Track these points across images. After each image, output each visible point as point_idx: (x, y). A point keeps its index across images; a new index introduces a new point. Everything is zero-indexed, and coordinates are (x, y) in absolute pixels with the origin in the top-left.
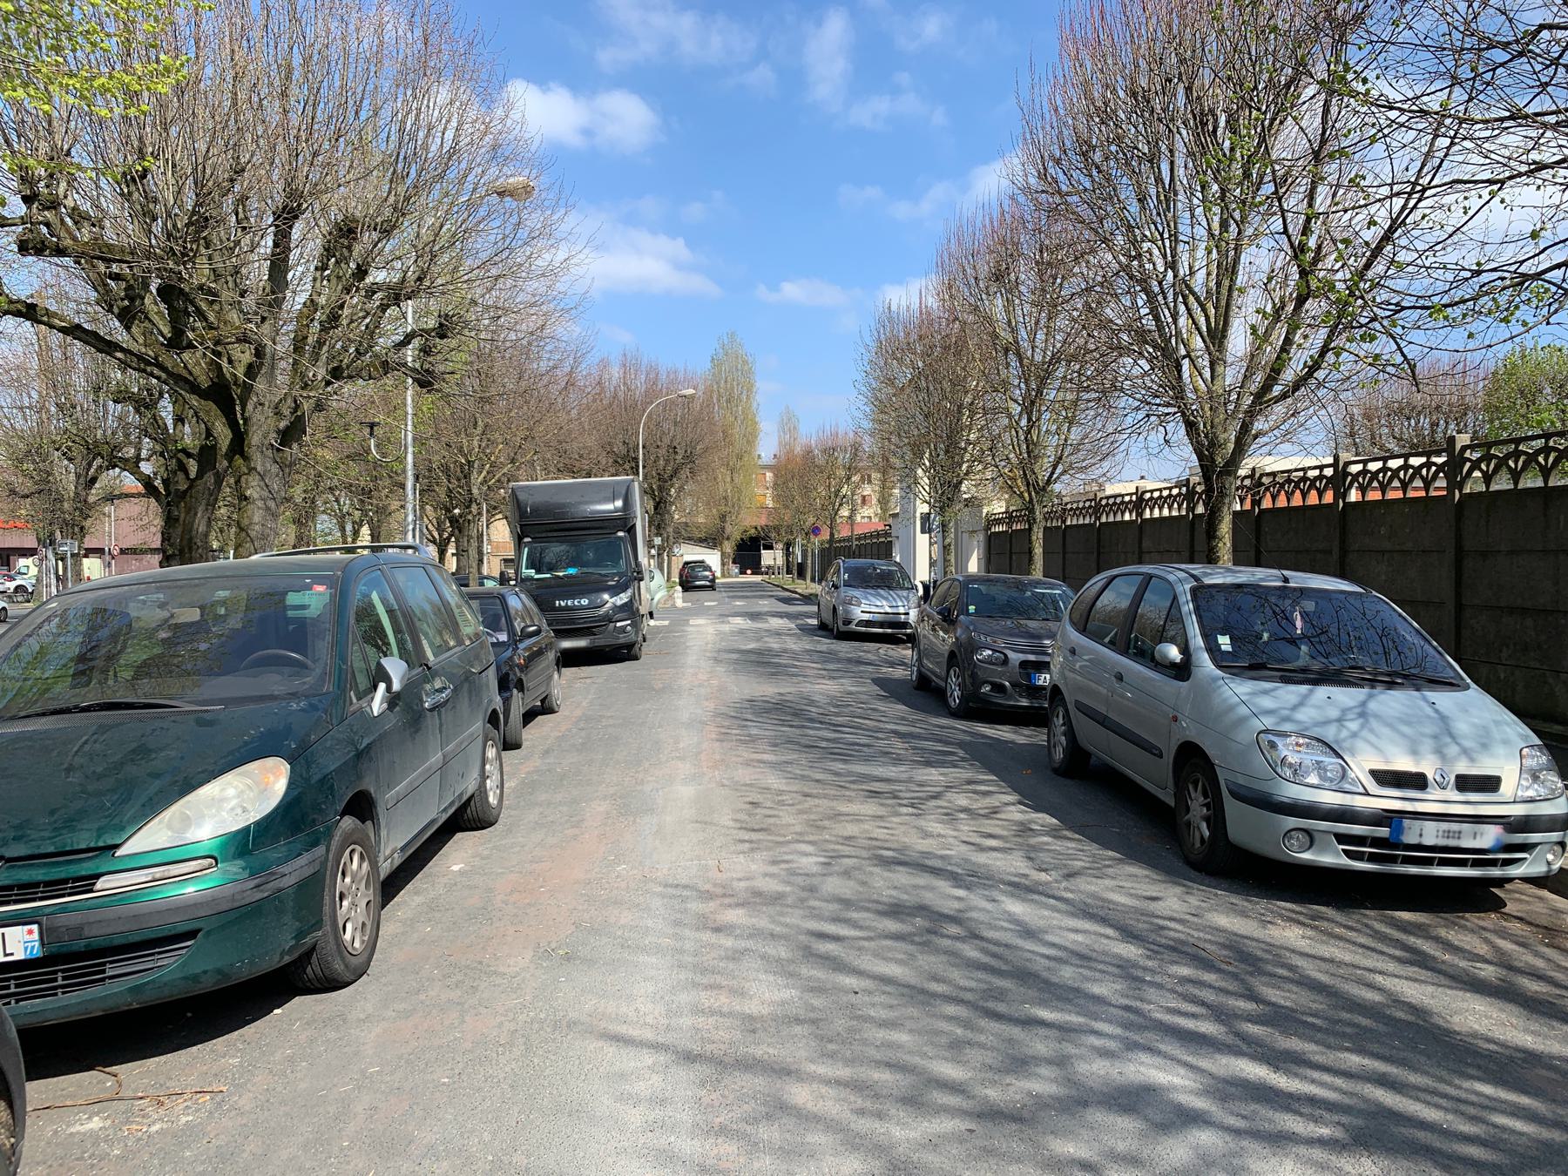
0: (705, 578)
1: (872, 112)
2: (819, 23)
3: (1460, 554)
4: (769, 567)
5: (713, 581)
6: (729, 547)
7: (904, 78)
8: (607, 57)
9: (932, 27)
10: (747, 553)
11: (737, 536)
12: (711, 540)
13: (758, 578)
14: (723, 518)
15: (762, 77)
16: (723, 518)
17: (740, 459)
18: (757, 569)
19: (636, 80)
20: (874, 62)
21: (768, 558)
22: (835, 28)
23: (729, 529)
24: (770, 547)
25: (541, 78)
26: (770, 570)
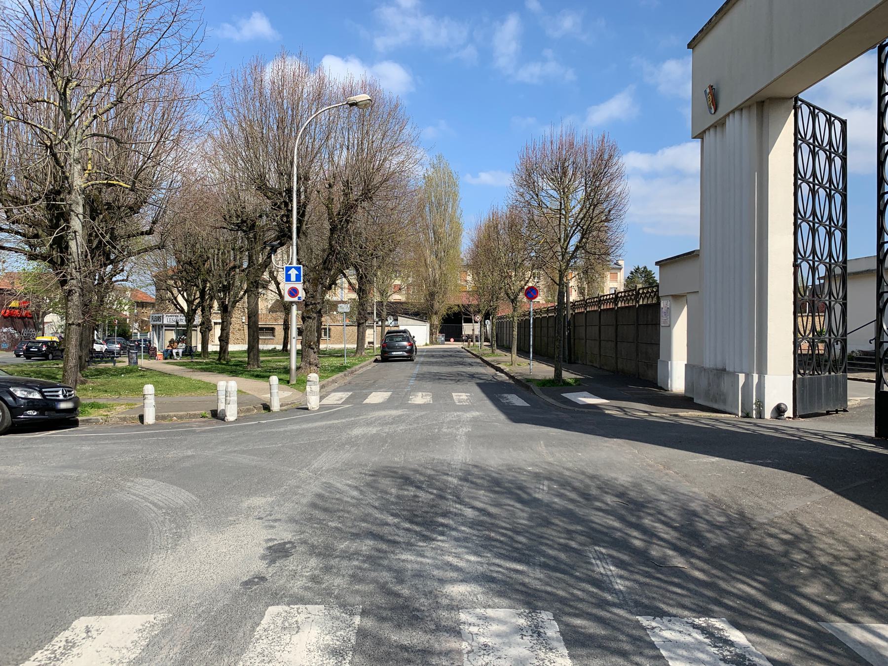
0: (402, 348)
1: (531, 73)
2: (503, 21)
3: (617, 326)
4: (468, 337)
5: (410, 351)
6: (436, 320)
7: (548, 53)
8: (381, 43)
9: (568, 22)
10: (451, 325)
11: (443, 312)
12: (420, 315)
13: (458, 345)
14: (432, 295)
15: (470, 53)
16: (432, 295)
17: (443, 246)
18: (458, 337)
19: (398, 56)
20: (533, 44)
21: (467, 329)
22: (512, 24)
23: (437, 306)
24: (469, 321)
25: (343, 54)
26: (469, 338)
